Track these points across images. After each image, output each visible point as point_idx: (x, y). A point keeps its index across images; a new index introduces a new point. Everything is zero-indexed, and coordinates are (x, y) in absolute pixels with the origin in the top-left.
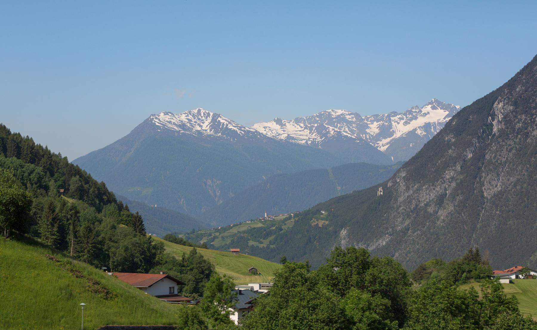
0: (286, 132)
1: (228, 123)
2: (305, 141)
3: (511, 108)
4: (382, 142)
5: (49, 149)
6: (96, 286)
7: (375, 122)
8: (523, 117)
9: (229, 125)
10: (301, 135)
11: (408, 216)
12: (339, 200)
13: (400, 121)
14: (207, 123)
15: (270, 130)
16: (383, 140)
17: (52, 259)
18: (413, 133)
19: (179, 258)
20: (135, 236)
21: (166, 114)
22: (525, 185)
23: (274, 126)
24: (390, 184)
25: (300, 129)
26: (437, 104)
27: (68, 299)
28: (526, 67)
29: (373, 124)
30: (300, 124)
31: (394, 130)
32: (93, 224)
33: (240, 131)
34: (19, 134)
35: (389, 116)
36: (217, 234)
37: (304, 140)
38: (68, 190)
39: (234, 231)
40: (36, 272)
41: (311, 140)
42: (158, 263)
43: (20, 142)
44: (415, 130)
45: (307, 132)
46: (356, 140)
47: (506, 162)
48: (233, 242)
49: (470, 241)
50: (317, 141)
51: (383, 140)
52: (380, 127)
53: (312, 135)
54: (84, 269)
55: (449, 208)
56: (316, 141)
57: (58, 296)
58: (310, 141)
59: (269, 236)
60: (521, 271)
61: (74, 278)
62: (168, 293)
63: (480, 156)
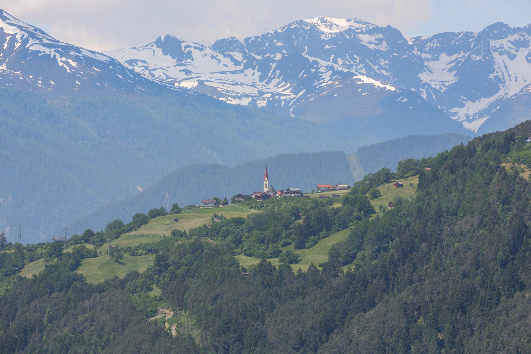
0: (193, 75)
1: (26, 35)
2: (250, 99)
4: (465, 108)
9: (31, 41)
10: (236, 84)
13: (517, 51)
16: (469, 104)
25: (232, 67)
29: (436, 59)
30: (231, 53)
31: (501, 77)
33: (64, 59)
37: (247, 96)
41: (265, 96)
46: (400, 95)
50: (285, 100)
53: (268, 83)
56: (280, 101)
59: (322, 234)
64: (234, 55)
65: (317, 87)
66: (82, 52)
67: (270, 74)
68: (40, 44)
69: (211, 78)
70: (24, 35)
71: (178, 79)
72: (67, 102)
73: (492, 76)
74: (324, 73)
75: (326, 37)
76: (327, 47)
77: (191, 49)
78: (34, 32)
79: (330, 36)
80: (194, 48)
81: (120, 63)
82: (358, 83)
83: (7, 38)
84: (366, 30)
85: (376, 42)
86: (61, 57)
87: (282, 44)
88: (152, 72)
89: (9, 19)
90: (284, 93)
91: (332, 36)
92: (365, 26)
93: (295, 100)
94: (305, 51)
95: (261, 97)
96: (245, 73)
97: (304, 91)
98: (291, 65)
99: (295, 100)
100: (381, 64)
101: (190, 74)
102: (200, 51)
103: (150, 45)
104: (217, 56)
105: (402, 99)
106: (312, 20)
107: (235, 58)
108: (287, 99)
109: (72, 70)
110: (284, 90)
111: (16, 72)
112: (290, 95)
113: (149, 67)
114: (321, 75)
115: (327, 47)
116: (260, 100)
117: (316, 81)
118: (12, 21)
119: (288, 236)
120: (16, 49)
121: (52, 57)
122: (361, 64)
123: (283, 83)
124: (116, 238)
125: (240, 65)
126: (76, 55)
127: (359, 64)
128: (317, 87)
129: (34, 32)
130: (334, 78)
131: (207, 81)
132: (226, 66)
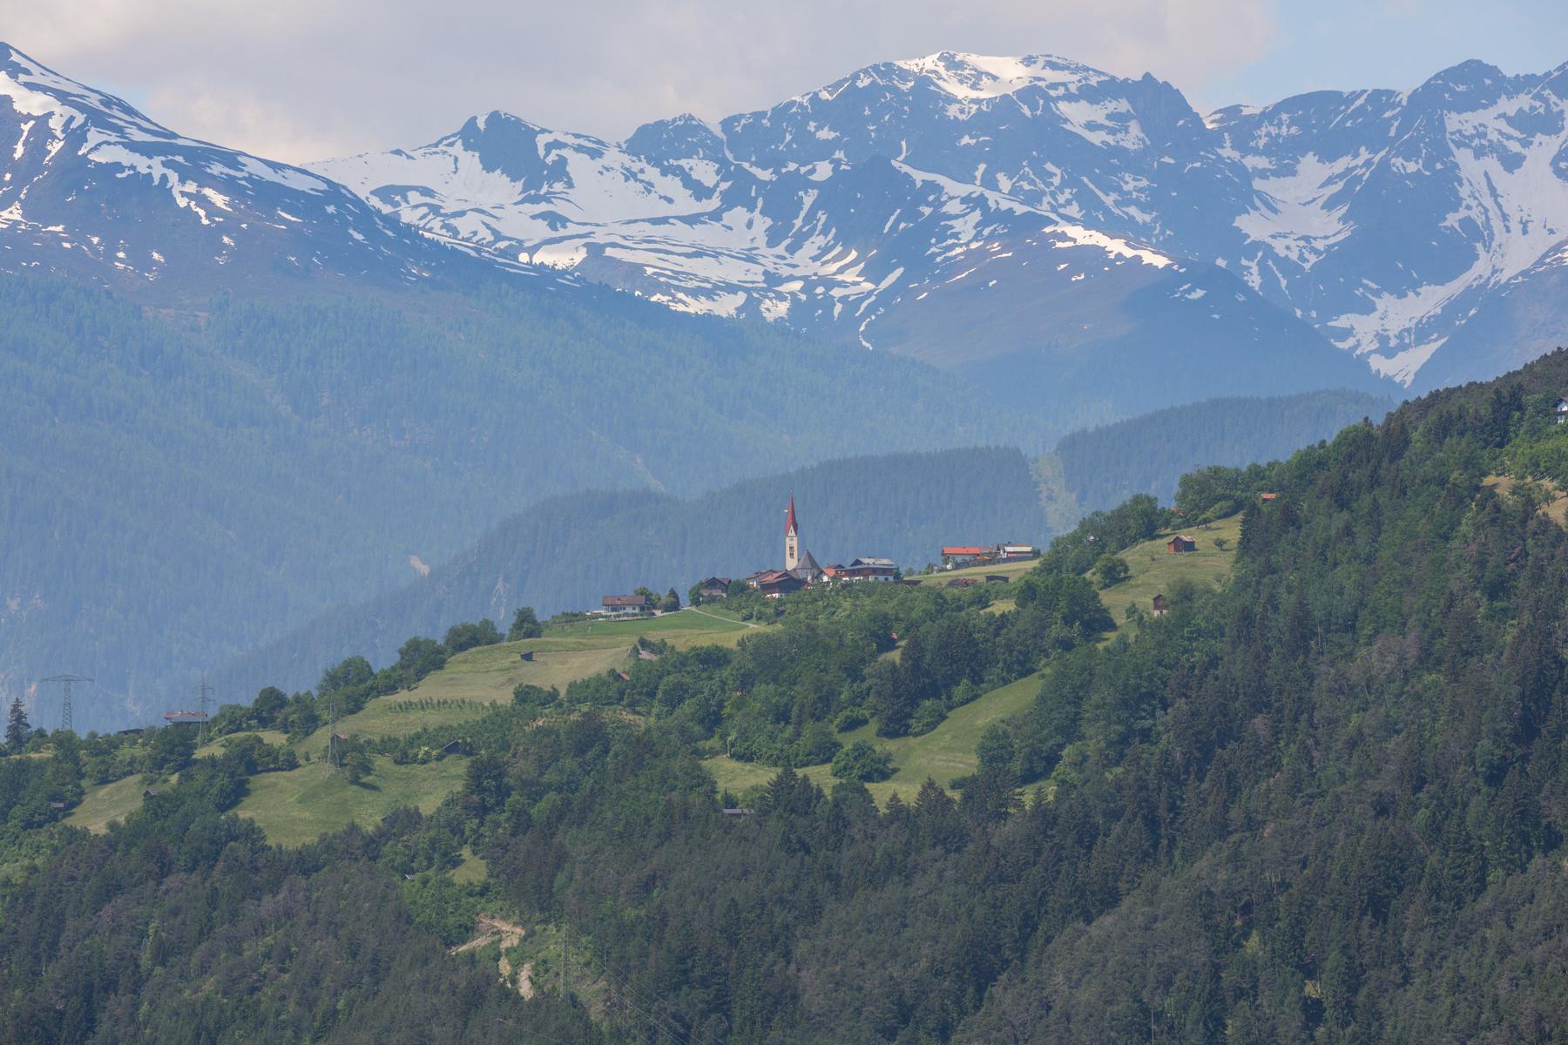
0: (572, 229)
1: (80, 119)
2: (741, 298)
4: (1375, 316)
7: (1309, 163)
9: (94, 136)
13: (1526, 144)
15: (435, 210)
16: (1385, 302)
25: (686, 204)
29: (1287, 171)
30: (684, 163)
33: (191, 187)
37: (731, 289)
46: (1183, 279)
50: (843, 299)
51: (1381, 304)
53: (792, 249)
56: (828, 302)
58: (781, 297)
59: (959, 691)
64: (691, 169)
65: (939, 259)
66: (245, 165)
67: (798, 223)
68: (119, 143)
69: (625, 238)
70: (72, 119)
71: (530, 240)
72: (202, 314)
73: (1452, 220)
74: (957, 217)
75: (962, 111)
76: (966, 140)
77: (565, 152)
78: (102, 108)
79: (975, 107)
80: (575, 149)
81: (355, 196)
82: (1060, 245)
83: (23, 126)
84: (1079, 89)
85: (1110, 124)
86: (182, 181)
87: (832, 135)
88: (453, 222)
89: (27, 72)
90: (839, 277)
91: (979, 109)
92: (1076, 77)
93: (873, 298)
94: (901, 153)
95: (774, 292)
96: (725, 222)
97: (899, 271)
98: (859, 195)
99: (873, 298)
100: (1126, 188)
101: (565, 227)
102: (592, 158)
103: (445, 142)
104: (642, 171)
105: (1189, 291)
106: (921, 62)
107: (695, 176)
108: (849, 296)
109: (217, 219)
110: (841, 270)
111: (50, 228)
112: (855, 284)
113: (441, 207)
114: (949, 223)
115: (966, 140)
116: (771, 299)
117: (933, 241)
118: (36, 78)
119: (858, 699)
120: (49, 161)
121: (156, 182)
122: (1067, 191)
123: (839, 249)
124: (352, 712)
125: (709, 197)
126: (227, 175)
127: (1061, 189)
128: (939, 259)
129: (102, 108)
130: (986, 232)
131: (614, 245)
132: (670, 201)
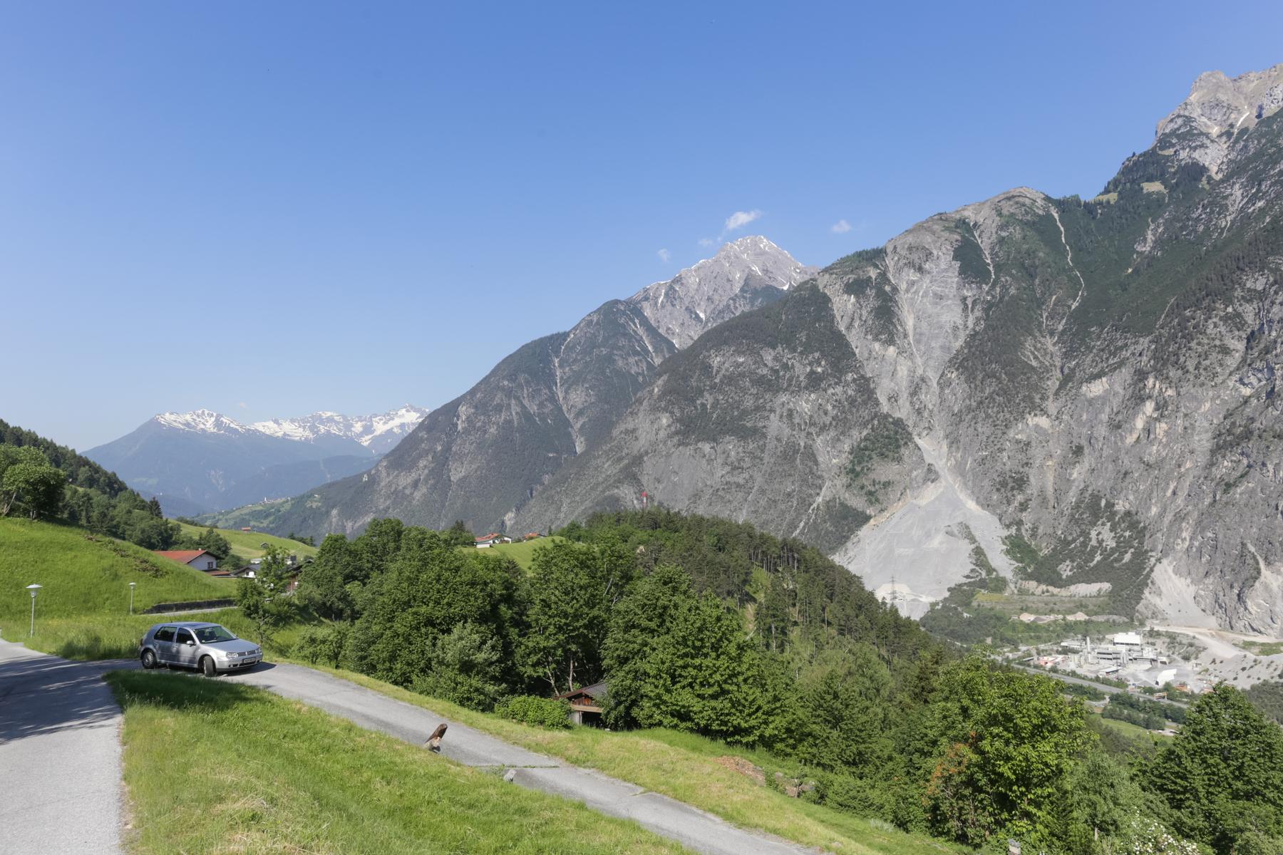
3: (473, 410)
5: (54, 441)
6: (144, 565)
8: (482, 417)
11: (389, 497)
12: (330, 485)
14: (210, 422)
17: (91, 539)
18: (390, 432)
19: (196, 538)
20: (152, 519)
21: (172, 414)
22: (484, 471)
23: (271, 424)
24: (373, 472)
25: (294, 427)
26: (412, 408)
27: (113, 580)
28: (485, 379)
32: (108, 509)
34: (20, 428)
35: (371, 417)
36: (221, 517)
38: (77, 479)
39: (237, 513)
40: (73, 553)
42: (175, 543)
43: (21, 435)
44: (392, 428)
45: (301, 430)
47: (468, 453)
48: (235, 523)
49: (440, 516)
52: (363, 426)
54: (129, 547)
55: (423, 490)
57: (101, 577)
60: (497, 538)
61: (118, 558)
62: (206, 568)
63: (447, 449)
